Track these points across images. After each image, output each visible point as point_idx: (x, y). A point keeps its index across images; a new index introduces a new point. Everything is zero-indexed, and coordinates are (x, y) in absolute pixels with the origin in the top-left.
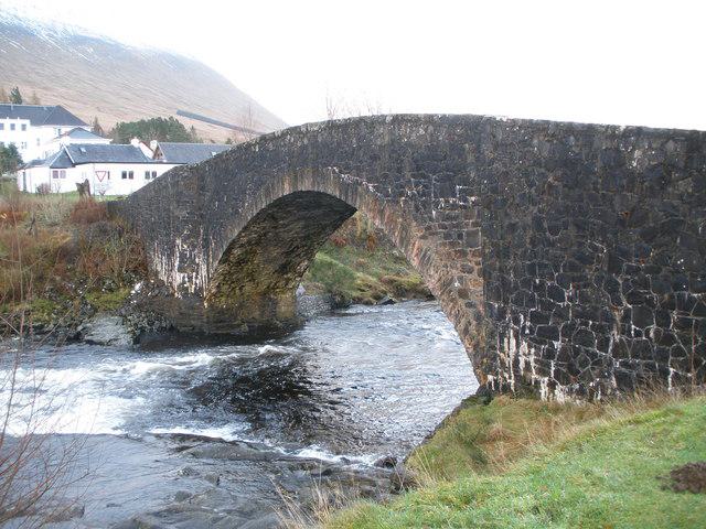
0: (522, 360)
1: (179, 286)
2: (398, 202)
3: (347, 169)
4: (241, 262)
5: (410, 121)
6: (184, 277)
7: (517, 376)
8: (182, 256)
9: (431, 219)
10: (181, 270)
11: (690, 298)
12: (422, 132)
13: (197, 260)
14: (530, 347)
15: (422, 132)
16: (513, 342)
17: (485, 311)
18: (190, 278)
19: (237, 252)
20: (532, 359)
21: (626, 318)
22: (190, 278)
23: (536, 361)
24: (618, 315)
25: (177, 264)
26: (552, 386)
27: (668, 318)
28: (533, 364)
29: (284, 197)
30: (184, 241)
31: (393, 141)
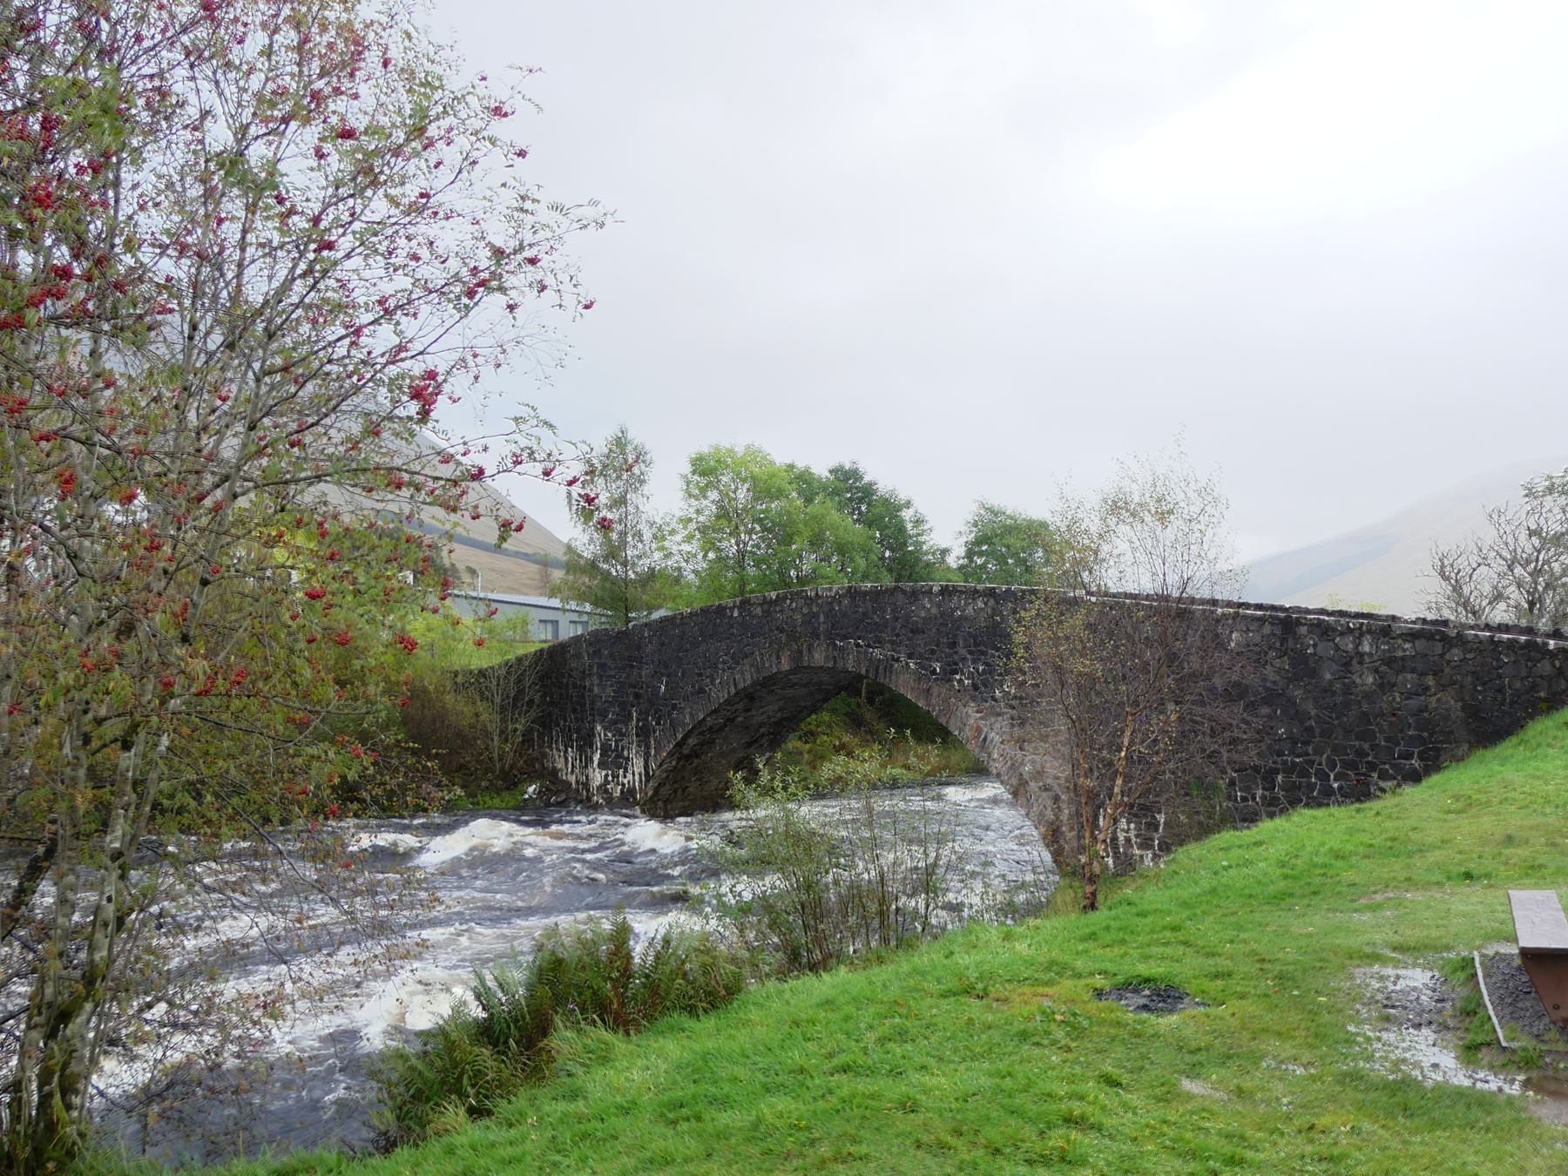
0: (1121, 837)
1: (599, 788)
2: (950, 680)
3: (879, 642)
4: (695, 754)
5: (963, 592)
6: (606, 776)
7: (1116, 855)
8: (605, 750)
9: (995, 700)
10: (602, 765)
11: (1293, 763)
12: (980, 604)
13: (626, 753)
14: (1129, 823)
15: (980, 604)
16: (237, 895)
17: (263, 904)
18: (615, 776)
19: (692, 741)
20: (1132, 834)
21: (1232, 783)
22: (615, 776)
23: (1137, 836)
24: (1222, 784)
25: (597, 757)
26: (1155, 857)
27: (1273, 781)
28: (1134, 840)
29: (779, 672)
30: (605, 729)
31: (942, 614)
